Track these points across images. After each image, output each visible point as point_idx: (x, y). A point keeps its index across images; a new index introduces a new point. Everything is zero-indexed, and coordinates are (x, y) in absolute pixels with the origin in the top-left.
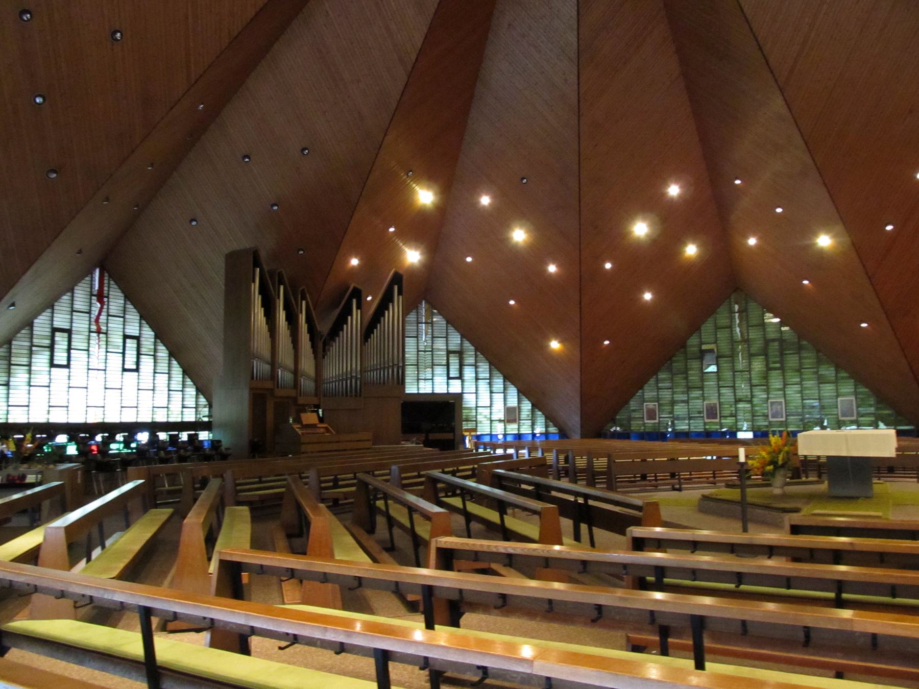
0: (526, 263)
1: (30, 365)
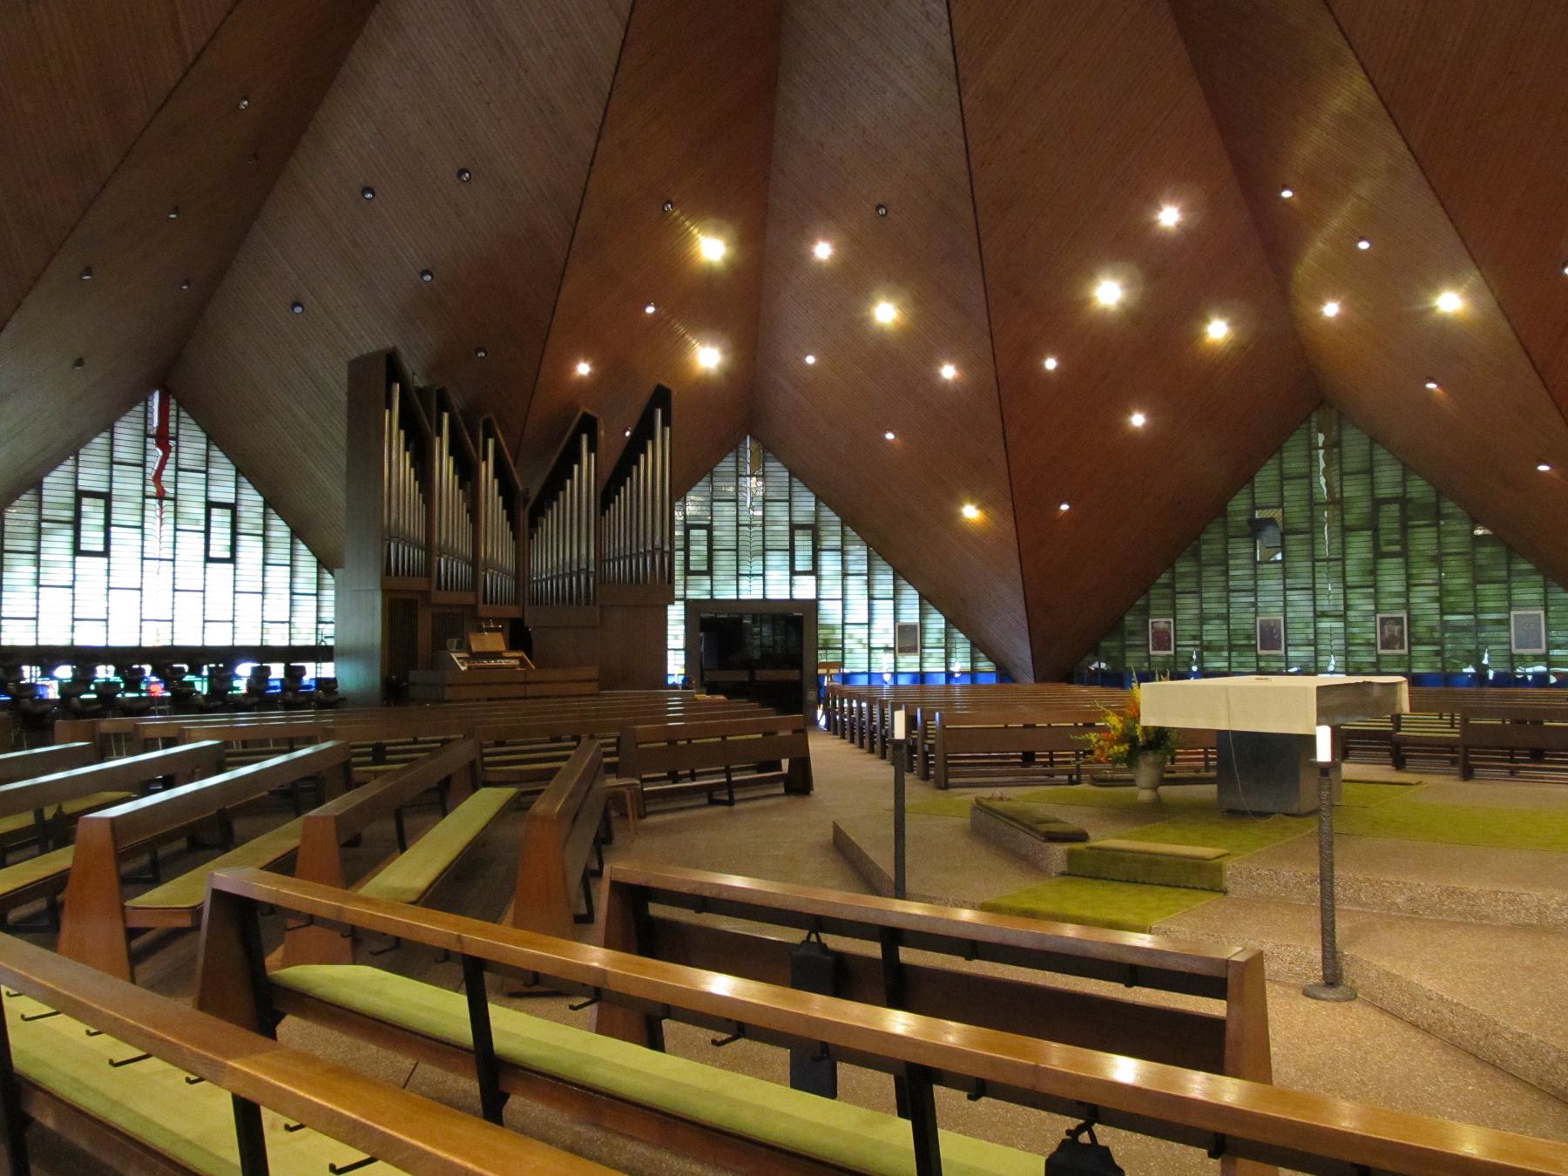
0: (900, 363)
1: (37, 552)
